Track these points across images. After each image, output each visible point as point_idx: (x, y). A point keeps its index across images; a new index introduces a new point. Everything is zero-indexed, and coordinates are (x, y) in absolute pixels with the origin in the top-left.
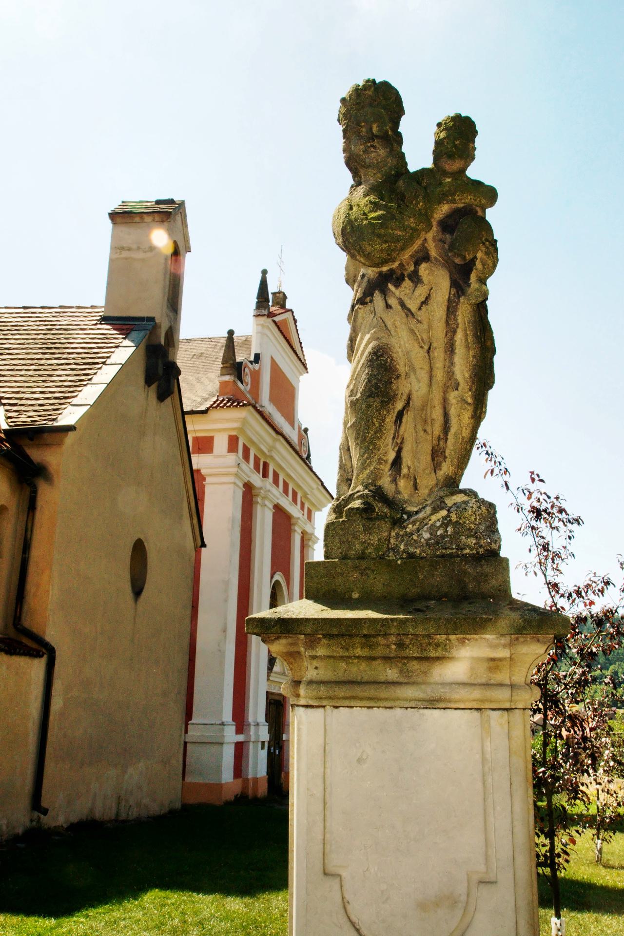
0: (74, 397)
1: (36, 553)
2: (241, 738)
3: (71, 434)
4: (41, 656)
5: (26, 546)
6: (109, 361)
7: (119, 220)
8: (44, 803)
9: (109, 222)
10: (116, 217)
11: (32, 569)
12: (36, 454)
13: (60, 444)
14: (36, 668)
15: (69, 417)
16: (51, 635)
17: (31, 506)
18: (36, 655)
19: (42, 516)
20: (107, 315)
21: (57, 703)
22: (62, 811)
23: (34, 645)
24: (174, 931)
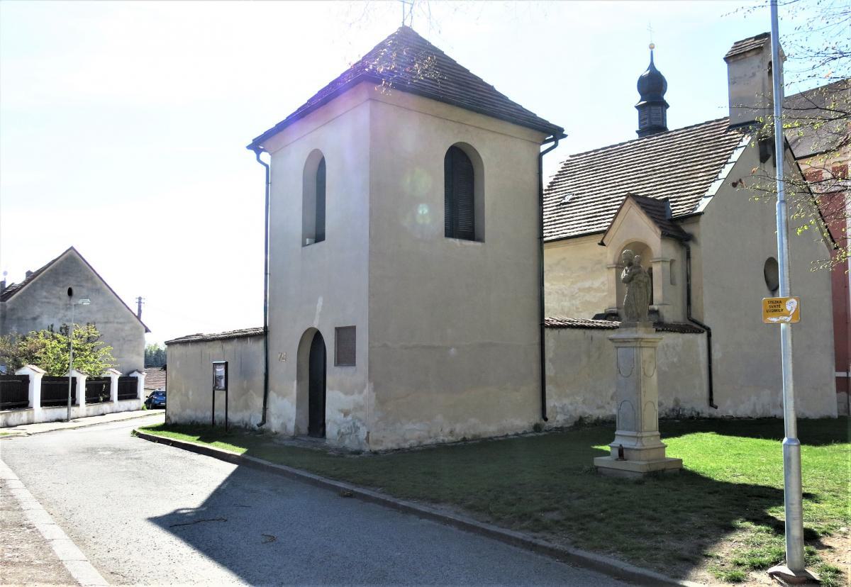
0: (706, 191)
1: (694, 280)
2: (843, 374)
3: (702, 216)
4: (703, 332)
5: (688, 278)
6: (729, 160)
7: (731, 61)
8: (715, 403)
9: (725, 65)
10: (257, 145)
11: (693, 288)
12: (687, 228)
13: (698, 222)
14: (701, 339)
15: (700, 209)
16: (707, 323)
17: (688, 256)
18: (700, 332)
19: (694, 261)
20: (732, 123)
21: (716, 355)
22: (558, 419)
23: (699, 327)
24: (3, 361)
